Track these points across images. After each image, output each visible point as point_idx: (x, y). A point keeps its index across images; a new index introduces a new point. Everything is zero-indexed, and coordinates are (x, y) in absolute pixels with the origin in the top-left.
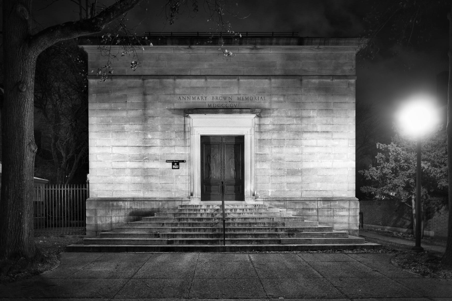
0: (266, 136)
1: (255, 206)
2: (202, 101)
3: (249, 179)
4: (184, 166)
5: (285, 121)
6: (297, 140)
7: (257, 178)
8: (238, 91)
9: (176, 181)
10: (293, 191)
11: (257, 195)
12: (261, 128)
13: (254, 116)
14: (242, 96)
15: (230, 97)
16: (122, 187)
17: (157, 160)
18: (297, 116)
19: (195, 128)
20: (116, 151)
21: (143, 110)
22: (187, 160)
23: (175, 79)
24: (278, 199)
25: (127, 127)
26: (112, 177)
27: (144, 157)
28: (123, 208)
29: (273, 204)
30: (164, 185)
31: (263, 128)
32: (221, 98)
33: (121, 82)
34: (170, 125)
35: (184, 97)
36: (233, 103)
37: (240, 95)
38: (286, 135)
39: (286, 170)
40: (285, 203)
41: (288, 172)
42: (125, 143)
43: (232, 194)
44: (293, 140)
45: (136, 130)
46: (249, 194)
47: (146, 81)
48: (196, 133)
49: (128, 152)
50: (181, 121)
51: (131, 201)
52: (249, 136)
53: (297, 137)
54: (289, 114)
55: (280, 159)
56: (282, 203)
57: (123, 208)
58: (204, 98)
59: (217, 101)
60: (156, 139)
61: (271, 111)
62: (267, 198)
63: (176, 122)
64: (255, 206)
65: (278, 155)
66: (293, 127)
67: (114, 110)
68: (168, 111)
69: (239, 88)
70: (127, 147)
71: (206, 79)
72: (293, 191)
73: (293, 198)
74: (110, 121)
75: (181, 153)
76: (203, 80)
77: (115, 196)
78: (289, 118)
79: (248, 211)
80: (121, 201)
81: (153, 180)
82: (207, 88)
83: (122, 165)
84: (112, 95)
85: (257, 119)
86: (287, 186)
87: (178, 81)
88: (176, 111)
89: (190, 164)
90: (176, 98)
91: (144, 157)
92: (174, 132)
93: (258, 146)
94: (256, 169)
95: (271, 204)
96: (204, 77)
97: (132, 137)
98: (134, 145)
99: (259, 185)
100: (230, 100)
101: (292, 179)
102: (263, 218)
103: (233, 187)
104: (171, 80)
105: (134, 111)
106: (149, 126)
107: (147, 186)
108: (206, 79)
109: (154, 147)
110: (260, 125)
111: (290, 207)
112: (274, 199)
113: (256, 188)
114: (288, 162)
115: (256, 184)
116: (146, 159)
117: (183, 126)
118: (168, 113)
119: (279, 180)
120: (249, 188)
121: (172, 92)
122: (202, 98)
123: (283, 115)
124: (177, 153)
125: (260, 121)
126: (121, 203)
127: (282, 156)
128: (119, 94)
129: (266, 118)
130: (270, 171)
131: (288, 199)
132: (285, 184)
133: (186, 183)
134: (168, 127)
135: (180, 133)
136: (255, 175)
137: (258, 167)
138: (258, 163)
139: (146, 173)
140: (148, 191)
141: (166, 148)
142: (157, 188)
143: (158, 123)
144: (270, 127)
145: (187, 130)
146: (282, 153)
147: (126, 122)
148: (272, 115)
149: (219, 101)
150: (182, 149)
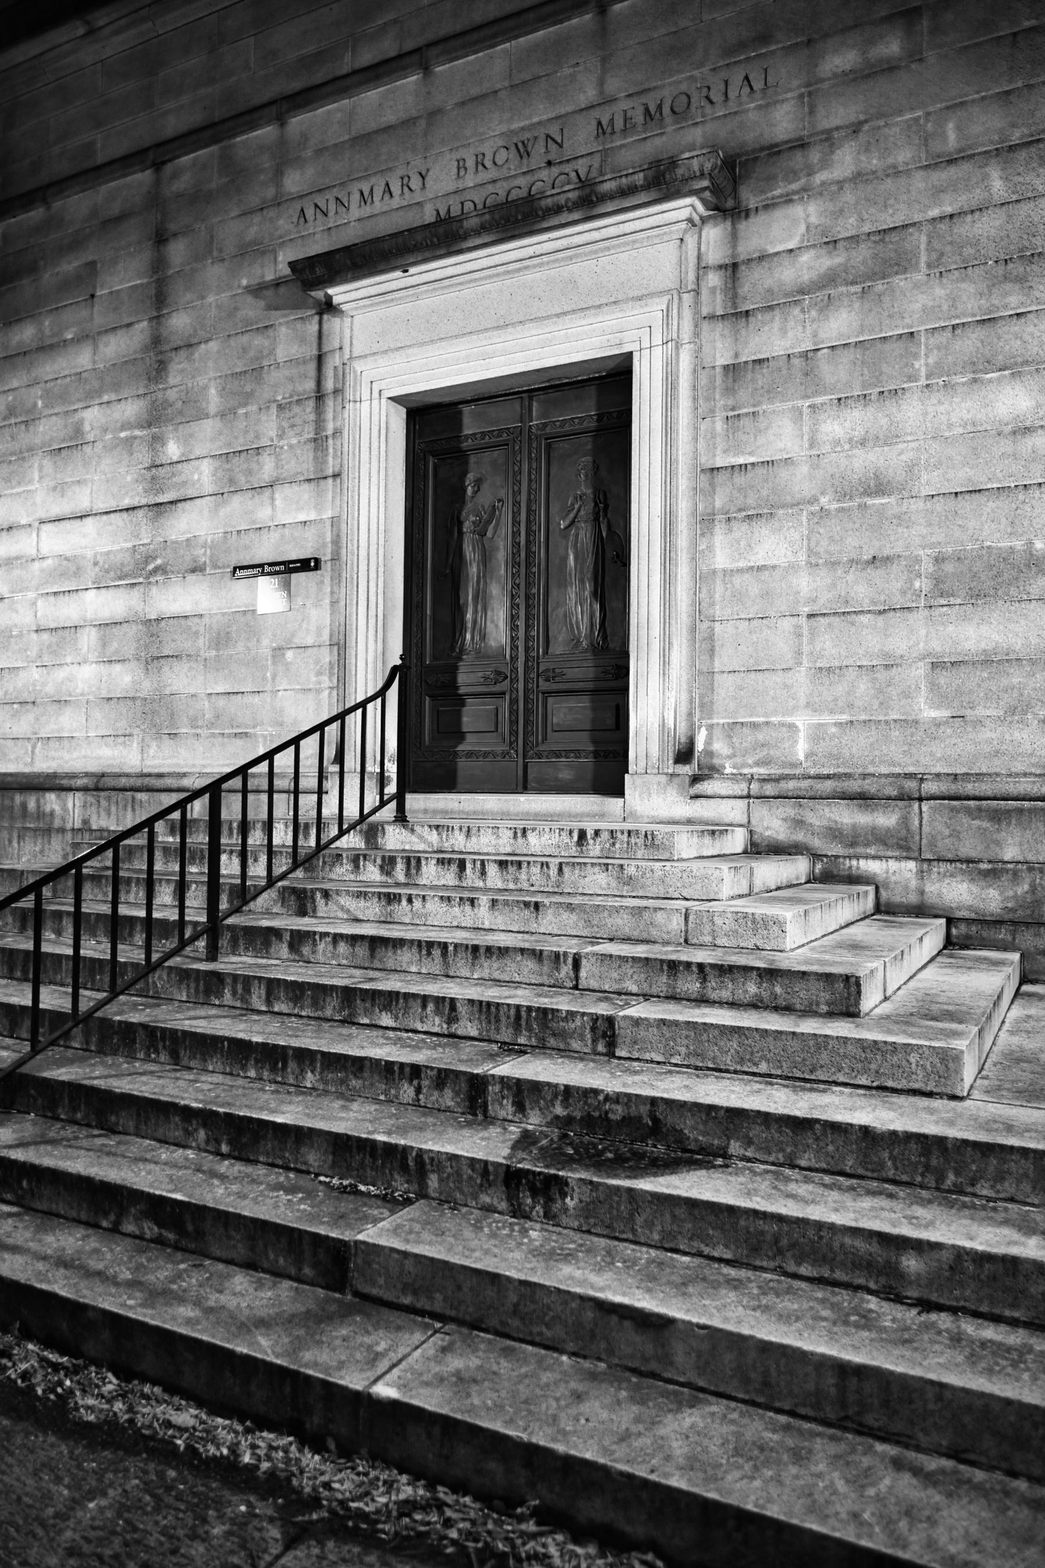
0: (776, 339)
1: (582, 834)
2: (409, 198)
3: (656, 645)
4: (313, 587)
5: (918, 200)
6: (1016, 326)
7: (711, 638)
8: (601, 82)
9: (274, 677)
10: (979, 723)
11: (709, 753)
12: (745, 289)
13: (684, 208)
14: (624, 105)
15: (554, 131)
16: (68, 722)
17: (197, 569)
18: (1016, 136)
19: (358, 366)
20: (55, 542)
21: (151, 319)
22: (326, 556)
23: (281, 120)
24: (854, 786)
25: (92, 417)
26: (36, 674)
27: (149, 558)
28: (57, 823)
29: (811, 818)
30: (221, 702)
31: (756, 283)
32: (502, 156)
33: (77, 205)
34: (256, 372)
35: (322, 205)
36: (567, 168)
37: (613, 100)
38: (919, 299)
39: (927, 566)
40: (905, 821)
41: (938, 581)
42: (82, 499)
43: (578, 753)
44: (980, 332)
45: (123, 428)
46: (655, 751)
47: (169, 168)
48: (366, 395)
49: (93, 540)
50: (303, 340)
51: (85, 789)
52: (658, 352)
53: (1015, 300)
54: (952, 139)
55: (879, 487)
56: (886, 819)
57: (57, 823)
58: (415, 183)
59: (484, 176)
60: (195, 452)
61: (815, 156)
62: (777, 780)
63: (282, 353)
64: (582, 834)
65: (864, 462)
66: (986, 227)
67: (51, 347)
68: (250, 299)
69: (604, 60)
70: (90, 519)
71: (426, 69)
72: (979, 723)
73: (980, 776)
74: (35, 405)
75: (302, 517)
76: (413, 79)
77: (43, 764)
78: (952, 172)
79: (494, 878)
80: (51, 789)
81: (180, 680)
82: (433, 115)
83: (68, 611)
84: (48, 278)
85: (714, 234)
86: (933, 686)
87: (298, 122)
88: (282, 290)
89: (337, 578)
90: (285, 223)
91: (149, 558)
92: (274, 409)
93: (720, 415)
94: (702, 578)
95: (799, 823)
96: (415, 58)
97: (107, 463)
98: (112, 505)
99: (725, 685)
100: (554, 154)
101: (975, 633)
102: (503, 952)
103: (583, 703)
104: (266, 133)
105: (120, 332)
106: (172, 395)
107: (156, 715)
108: (426, 69)
109: (188, 505)
110: (732, 269)
111: (946, 846)
112: (828, 786)
113: (701, 703)
114: (939, 505)
115: (704, 678)
116: (156, 570)
117: (311, 368)
118: (252, 309)
119: (871, 639)
120: (653, 708)
121: (270, 192)
122: (406, 185)
123: (903, 156)
124: (289, 518)
125: (734, 237)
126: (51, 801)
127: (890, 460)
128: (69, 266)
129: (778, 213)
130: (804, 583)
131: (930, 787)
132: (920, 671)
133: (319, 691)
134: (248, 388)
135: (296, 409)
136: (699, 613)
137: (721, 560)
138: (719, 529)
139: (153, 643)
140: (158, 736)
141: (236, 499)
142: (193, 723)
143: (202, 375)
144: (811, 265)
145: (329, 385)
146: (890, 439)
147: (91, 396)
148: (819, 178)
149: (492, 173)
150: (306, 491)
